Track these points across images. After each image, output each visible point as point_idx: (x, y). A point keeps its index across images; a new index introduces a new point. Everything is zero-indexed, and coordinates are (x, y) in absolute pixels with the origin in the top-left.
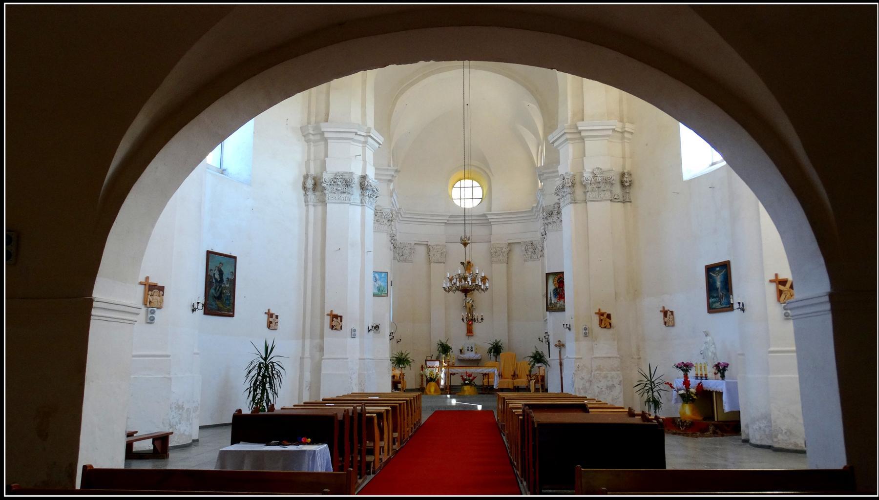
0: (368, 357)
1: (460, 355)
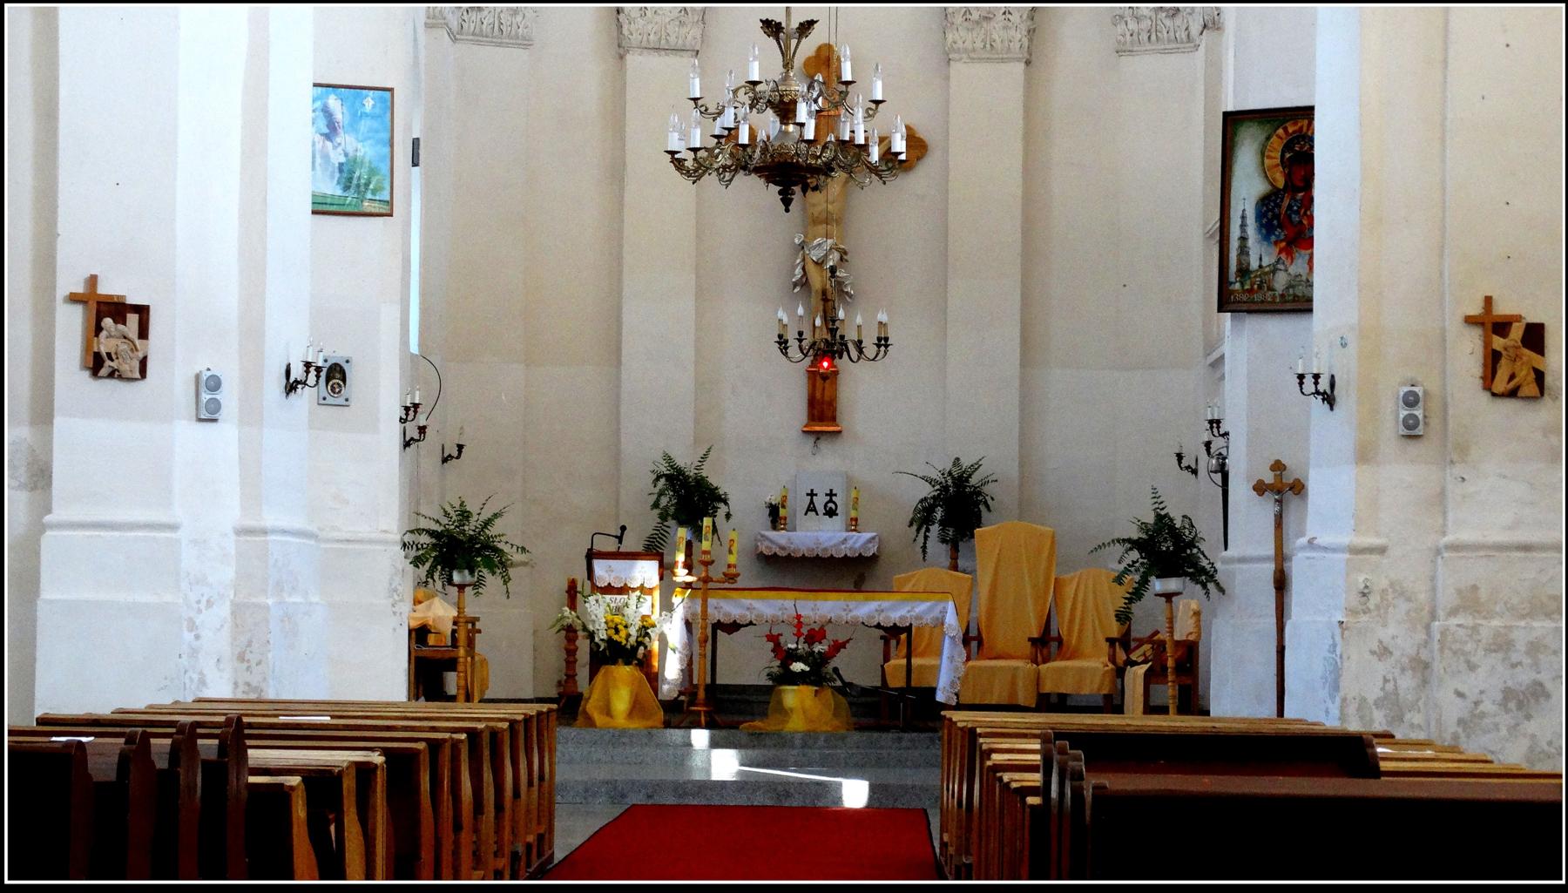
0: (284, 523)
1: (772, 534)
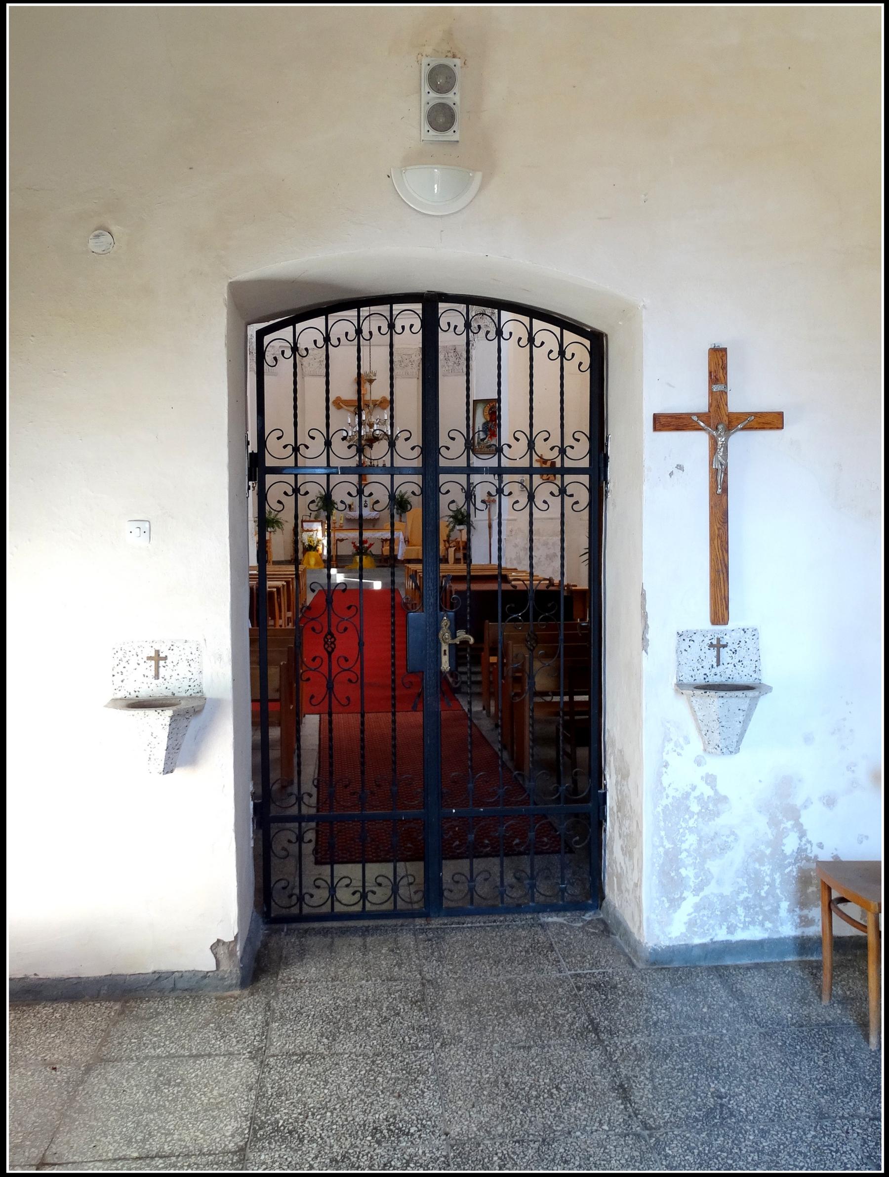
1: (350, 513)
